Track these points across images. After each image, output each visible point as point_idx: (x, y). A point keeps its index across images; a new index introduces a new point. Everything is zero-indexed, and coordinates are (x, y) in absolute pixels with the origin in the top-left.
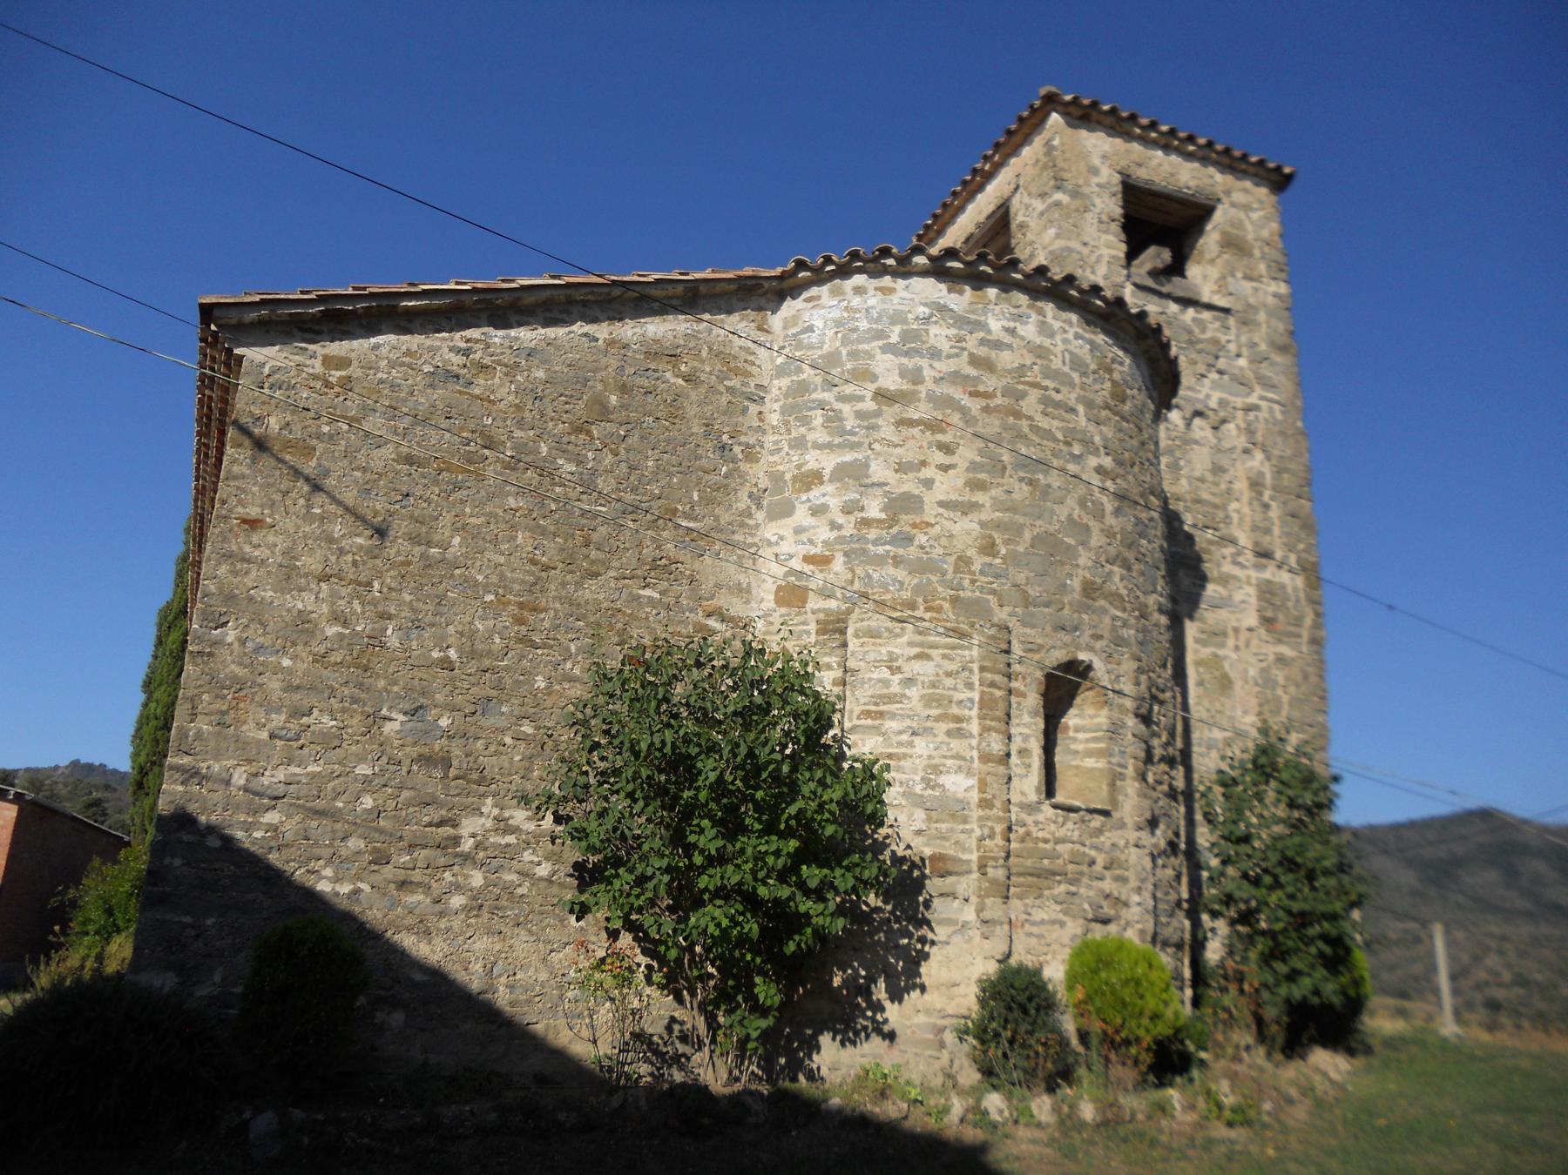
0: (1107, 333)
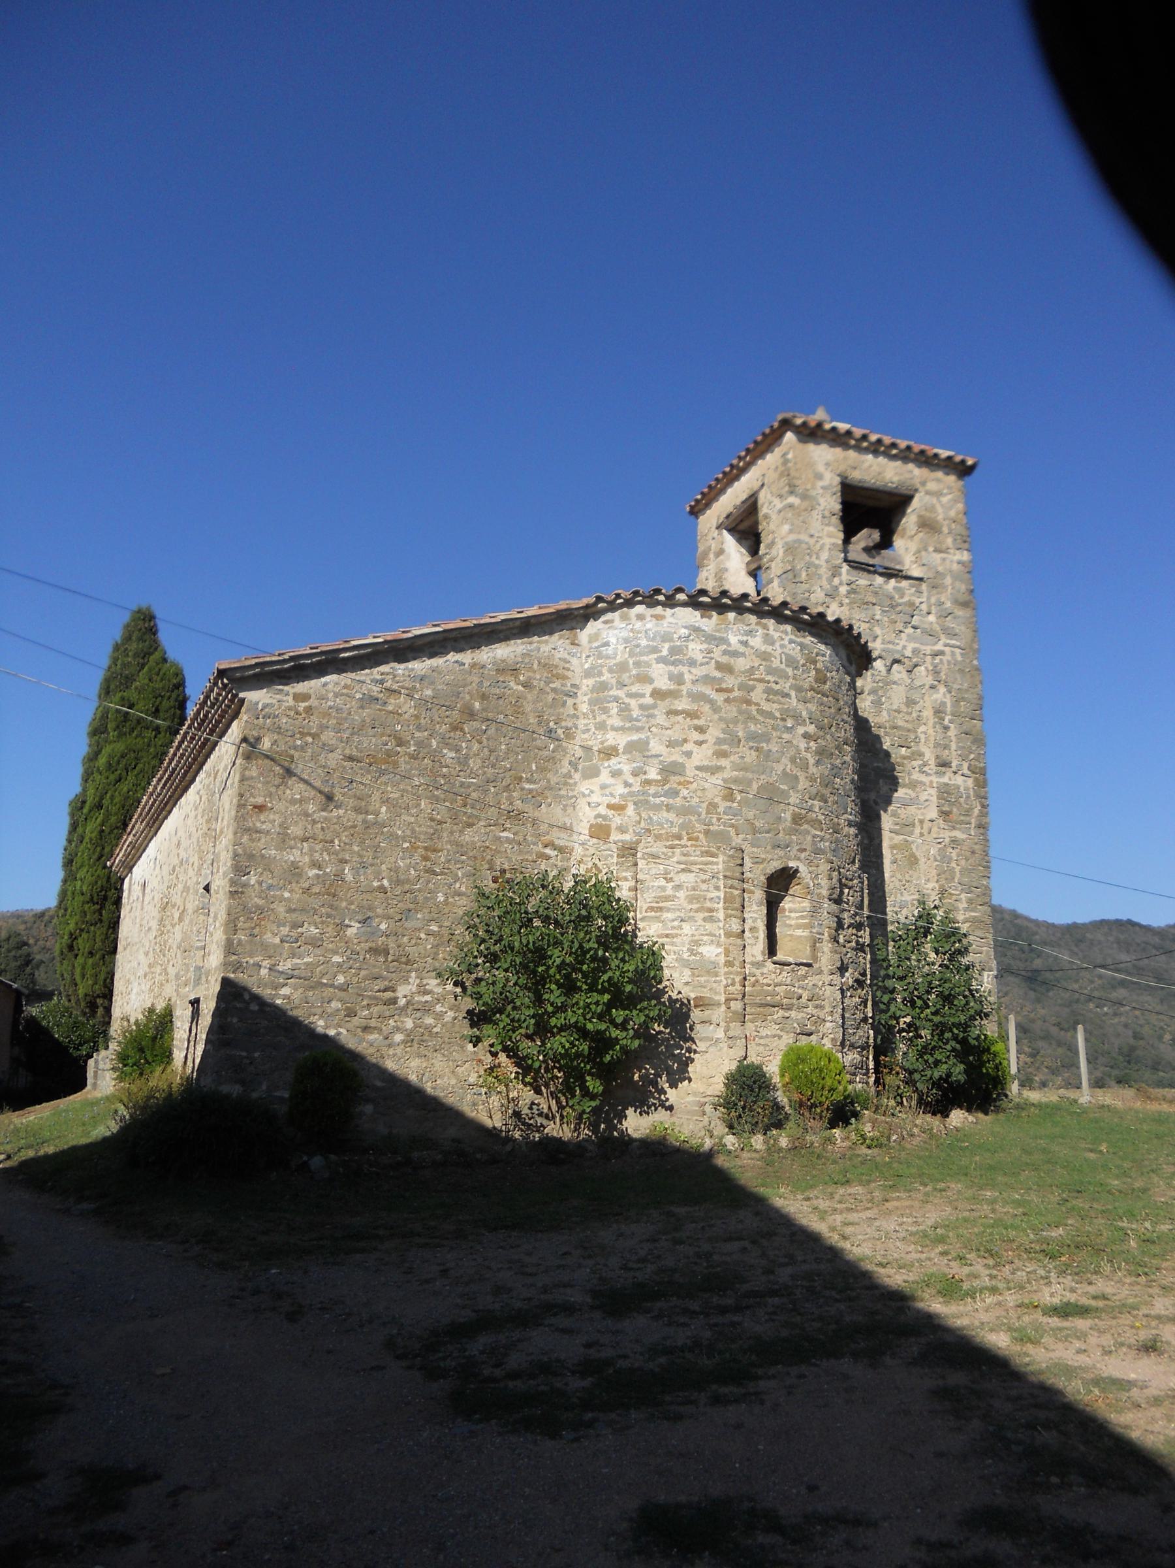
0: (812, 635)
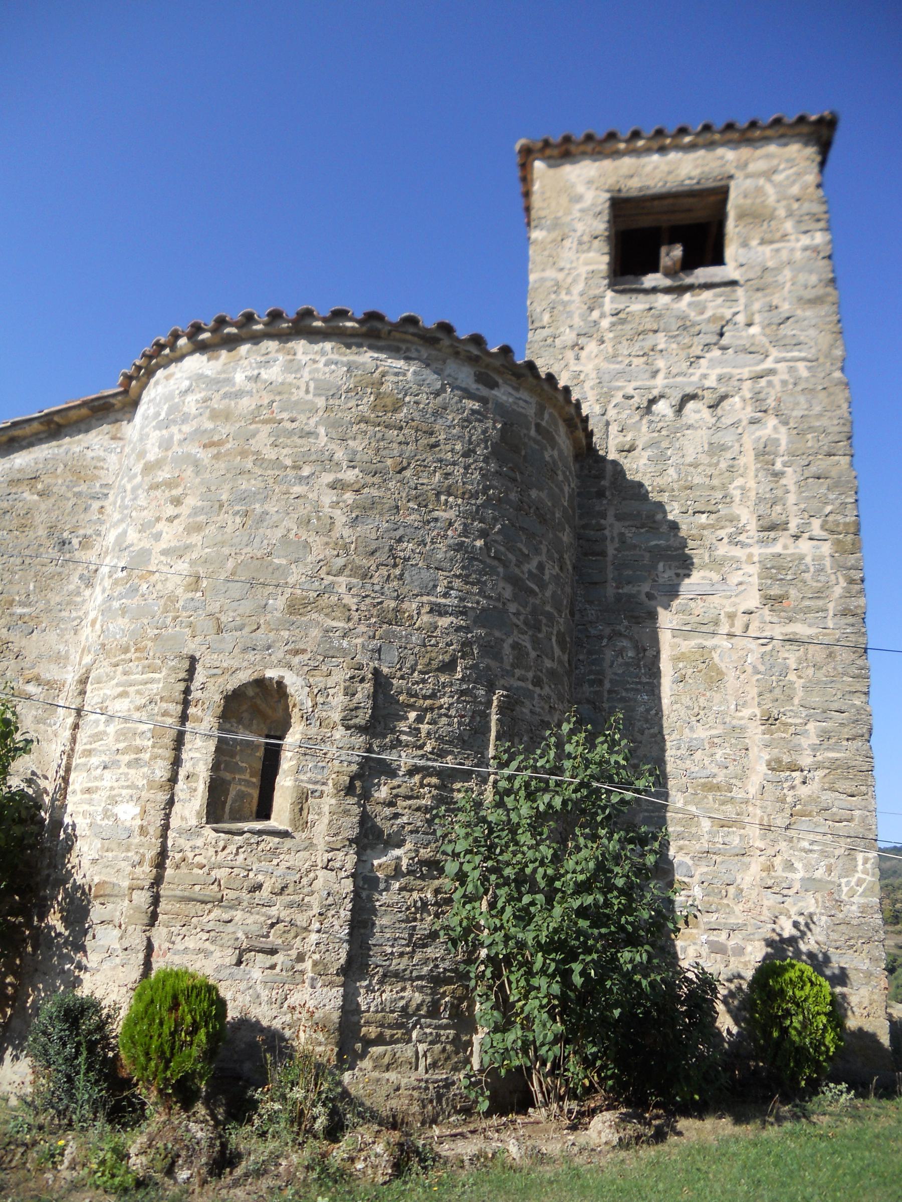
0: (371, 347)
